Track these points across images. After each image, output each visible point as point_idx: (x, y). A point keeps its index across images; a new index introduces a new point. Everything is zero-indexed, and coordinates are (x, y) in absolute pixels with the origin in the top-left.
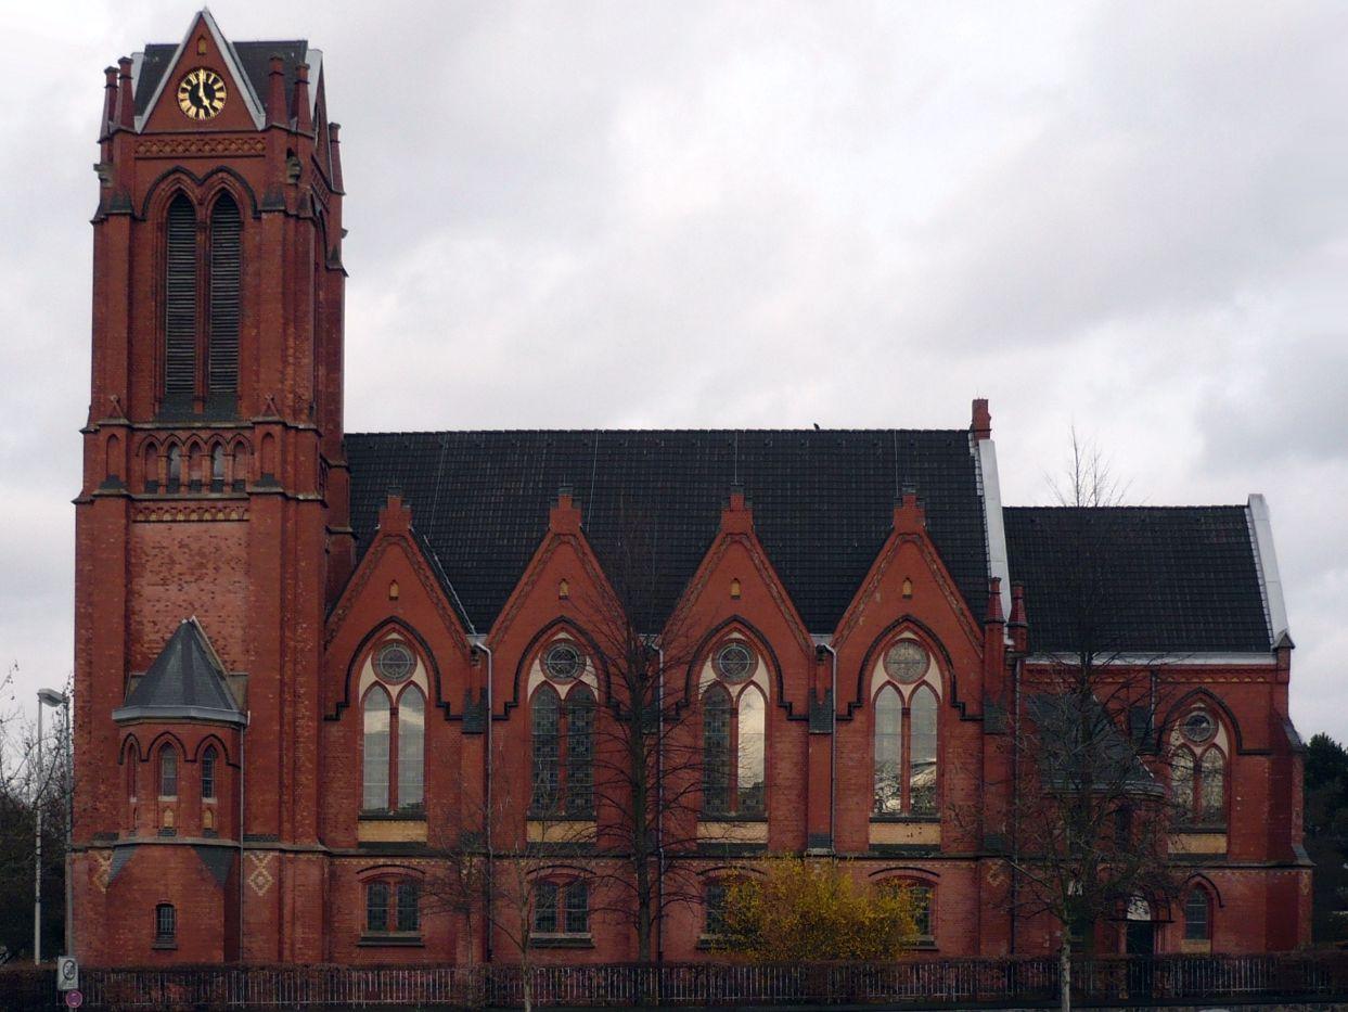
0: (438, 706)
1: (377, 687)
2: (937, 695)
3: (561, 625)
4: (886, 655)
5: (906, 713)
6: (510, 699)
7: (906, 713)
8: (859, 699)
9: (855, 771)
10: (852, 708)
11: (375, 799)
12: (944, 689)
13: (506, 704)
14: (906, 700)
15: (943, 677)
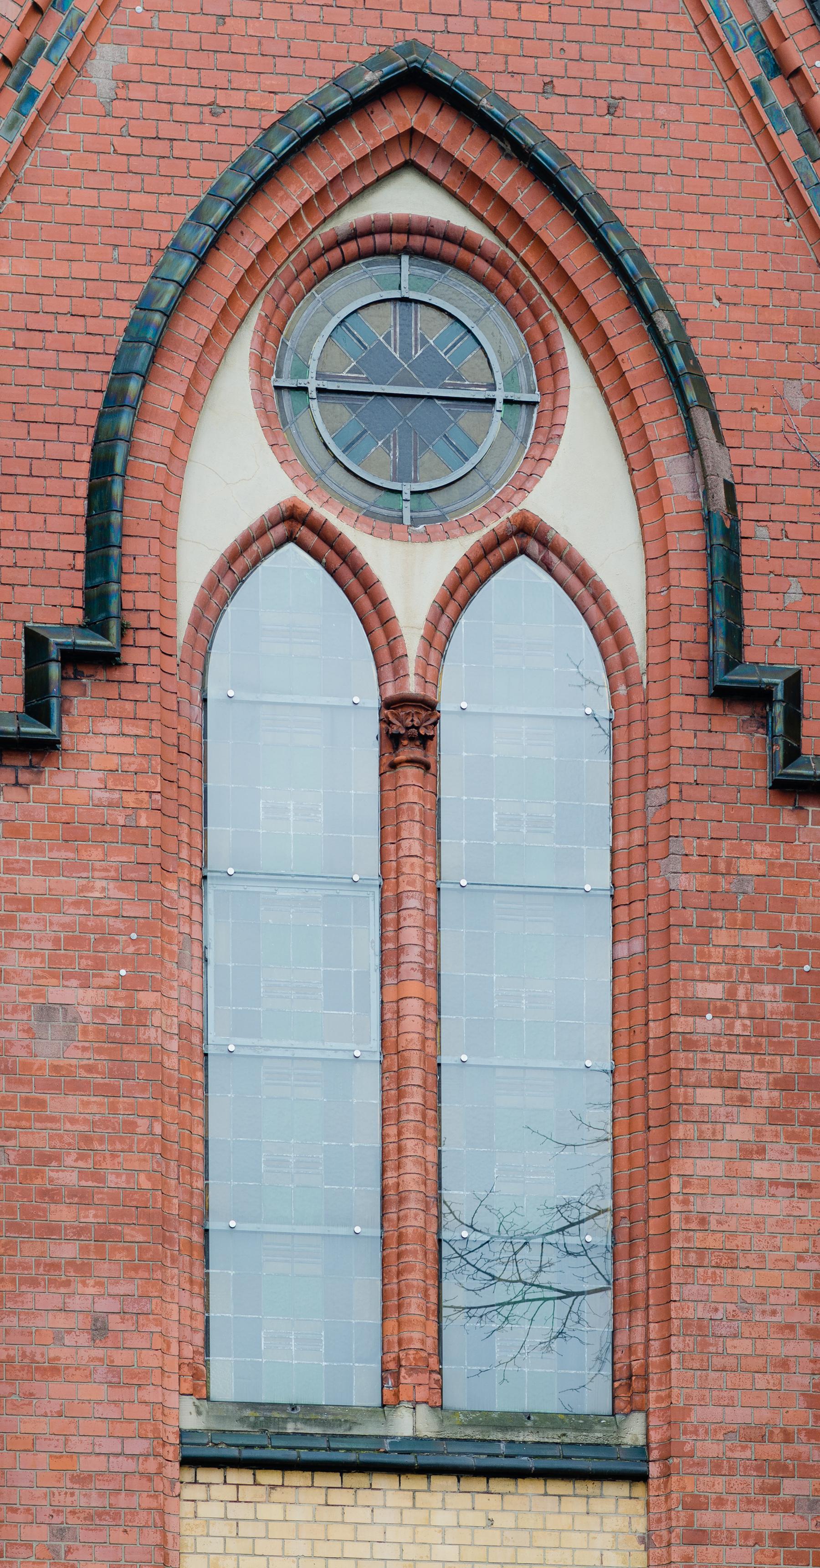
0: (726, 695)
1: (292, 563)
2: (607, 628)
3: (388, 122)
4: (274, 332)
5: (409, 730)
6: (57, 609)
7: (409, 730)
8: (97, 607)
9: (73, 1103)
10: (61, 665)
11: (292, 1329)
12: (657, 564)
13: (35, 644)
14: (412, 643)
15: (648, 490)
